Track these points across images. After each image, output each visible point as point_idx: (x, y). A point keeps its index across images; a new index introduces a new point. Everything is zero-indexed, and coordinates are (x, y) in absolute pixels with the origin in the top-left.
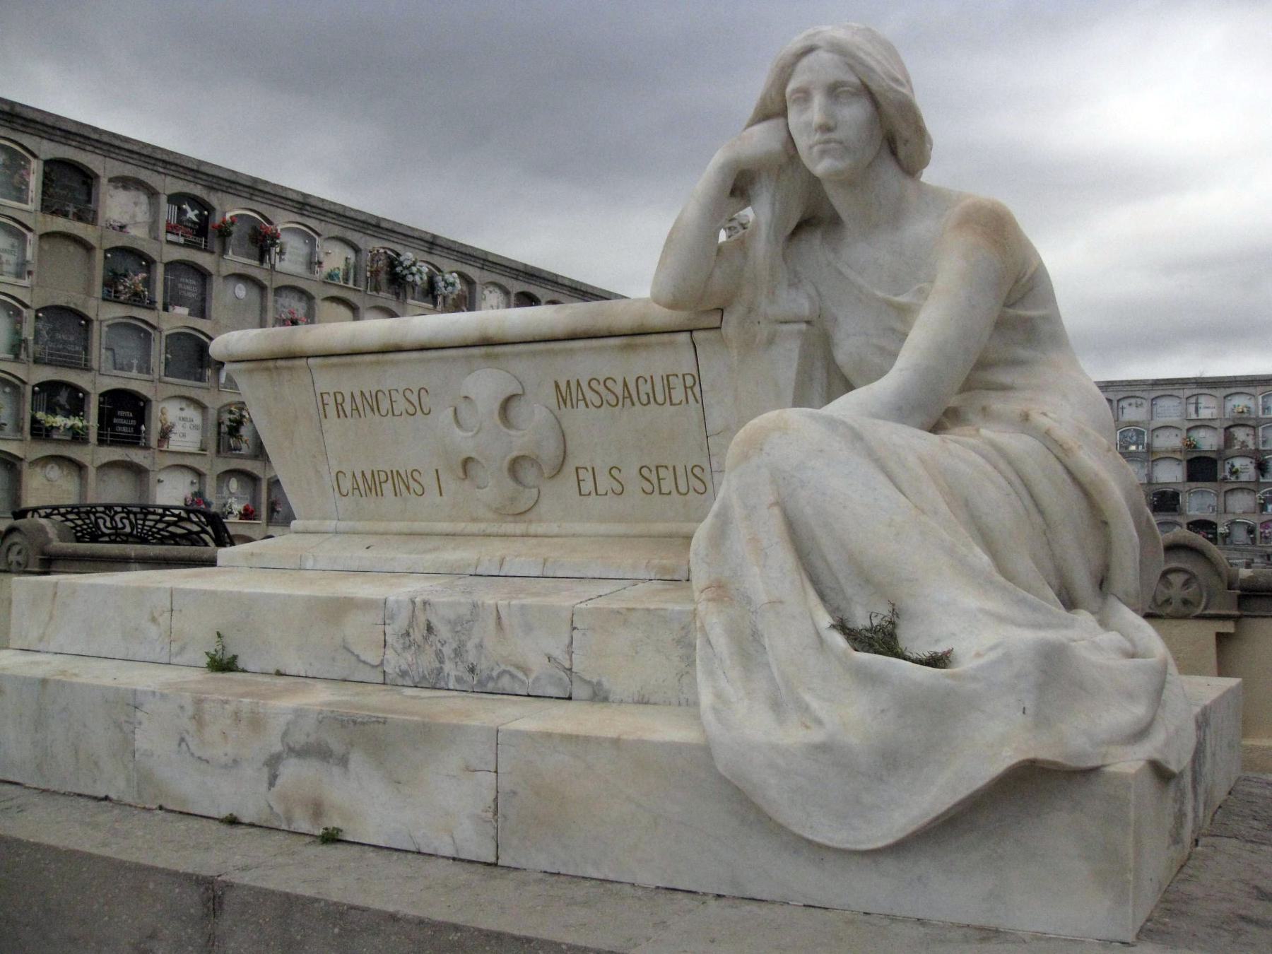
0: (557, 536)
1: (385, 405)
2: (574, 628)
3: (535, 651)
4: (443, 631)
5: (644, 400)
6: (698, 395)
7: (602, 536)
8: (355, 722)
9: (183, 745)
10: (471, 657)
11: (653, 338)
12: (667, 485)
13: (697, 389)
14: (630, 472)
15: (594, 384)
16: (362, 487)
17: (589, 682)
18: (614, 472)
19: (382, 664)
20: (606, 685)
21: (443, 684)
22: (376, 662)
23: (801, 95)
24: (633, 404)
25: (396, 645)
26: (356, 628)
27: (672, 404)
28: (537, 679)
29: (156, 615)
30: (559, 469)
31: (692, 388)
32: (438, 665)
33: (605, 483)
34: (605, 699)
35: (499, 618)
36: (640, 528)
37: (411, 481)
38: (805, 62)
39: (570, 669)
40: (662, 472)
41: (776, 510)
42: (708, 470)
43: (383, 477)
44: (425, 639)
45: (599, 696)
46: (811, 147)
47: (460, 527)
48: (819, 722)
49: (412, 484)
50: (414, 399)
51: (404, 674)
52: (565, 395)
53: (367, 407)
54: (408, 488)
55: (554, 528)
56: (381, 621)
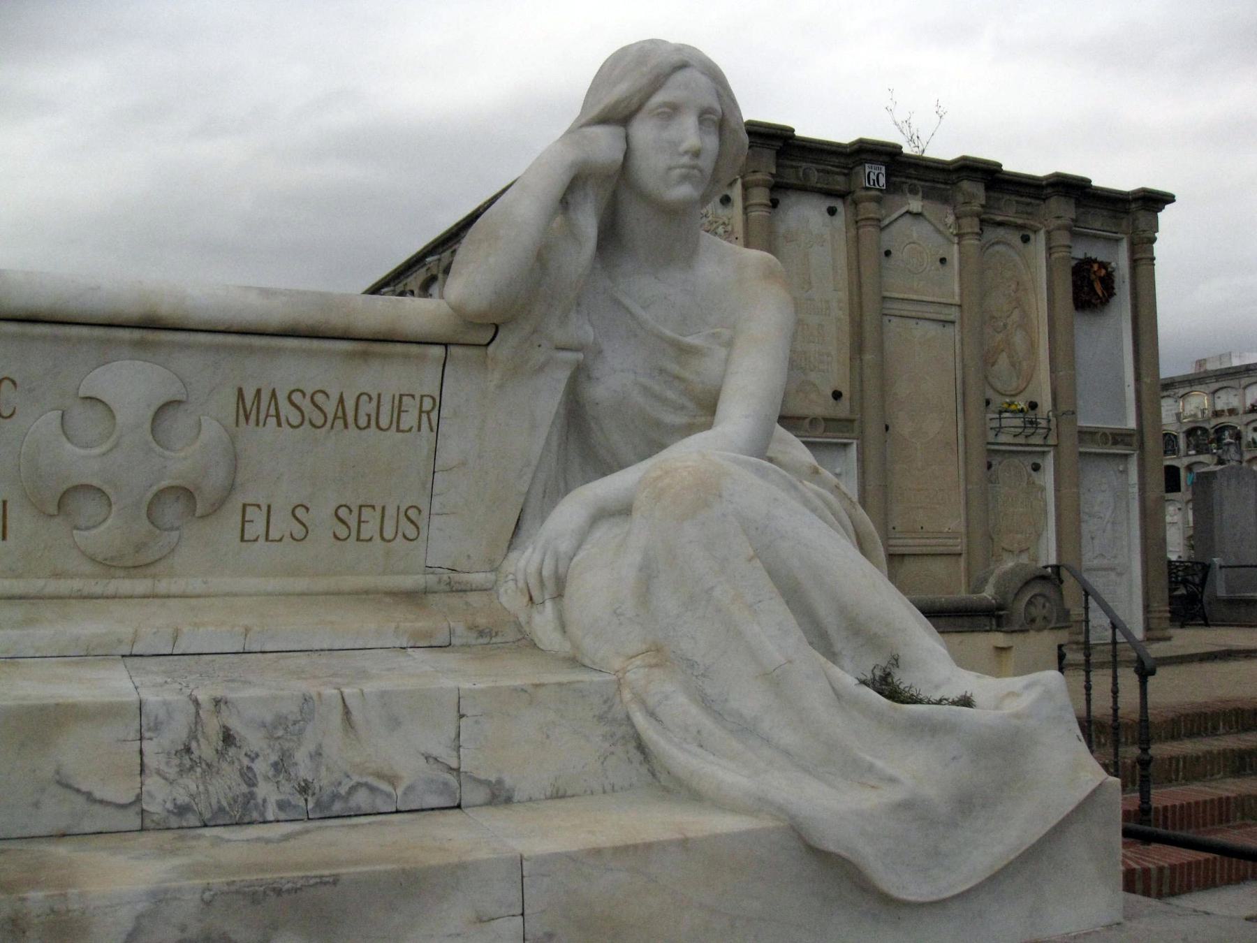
0: (199, 596)
2: (462, 716)
3: (404, 755)
4: (253, 740)
5: (363, 421)
8: (279, 892)
10: (303, 770)
11: (399, 348)
12: (370, 529)
14: (321, 514)
15: (297, 397)
17: (487, 783)
18: (300, 512)
19: (139, 799)
20: (508, 782)
21: (255, 815)
22: (132, 798)
23: (666, 110)
24: (346, 426)
25: (163, 767)
26: (74, 753)
27: (398, 430)
28: (410, 789)
30: (218, 506)
31: (428, 413)
32: (244, 788)
34: (508, 800)
35: (347, 712)
36: (323, 584)
38: (680, 77)
39: (458, 770)
40: (366, 513)
41: (757, 563)
42: (425, 513)
44: (221, 754)
45: (499, 796)
46: (670, 169)
48: (892, 780)
51: (182, 810)
52: (248, 409)
55: (196, 585)
56: (133, 735)
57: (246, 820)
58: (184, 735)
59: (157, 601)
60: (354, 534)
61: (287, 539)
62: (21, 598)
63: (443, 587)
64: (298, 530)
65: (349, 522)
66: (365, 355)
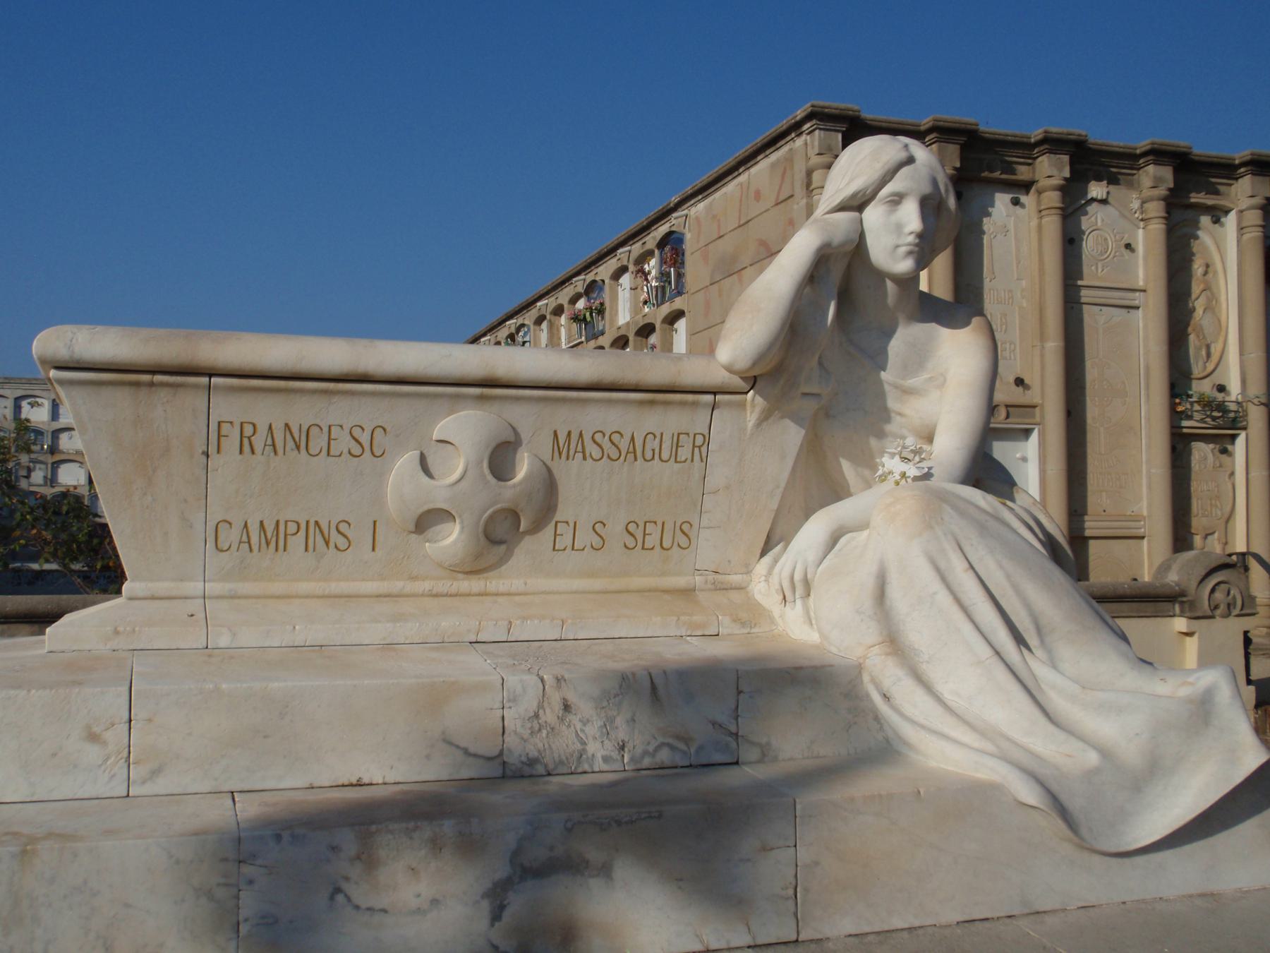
1: (319, 442)
2: (739, 692)
5: (649, 455)
6: (704, 455)
7: (575, 592)
8: (619, 823)
9: (340, 898)
13: (704, 449)
14: (615, 528)
15: (598, 437)
16: (255, 540)
21: (586, 767)
25: (519, 730)
27: (676, 461)
29: (96, 729)
31: (700, 447)
32: (579, 746)
33: (585, 537)
37: (333, 531)
39: (737, 734)
42: (696, 526)
43: (292, 528)
44: (561, 719)
47: (397, 586)
49: (335, 538)
50: (365, 439)
53: (290, 444)
54: (327, 543)
56: (498, 705)
57: (580, 770)
58: (534, 705)
59: (489, 599)
60: (640, 544)
61: (346, 455)
62: (385, 596)
63: (710, 586)
64: (597, 541)
65: (635, 535)
66: (652, 403)
